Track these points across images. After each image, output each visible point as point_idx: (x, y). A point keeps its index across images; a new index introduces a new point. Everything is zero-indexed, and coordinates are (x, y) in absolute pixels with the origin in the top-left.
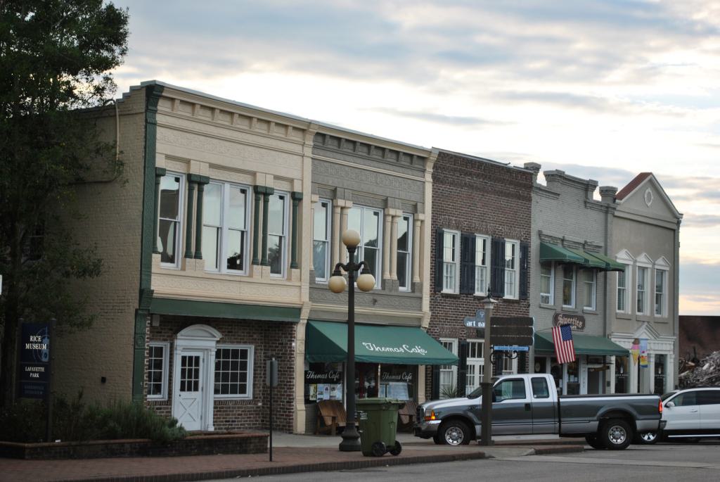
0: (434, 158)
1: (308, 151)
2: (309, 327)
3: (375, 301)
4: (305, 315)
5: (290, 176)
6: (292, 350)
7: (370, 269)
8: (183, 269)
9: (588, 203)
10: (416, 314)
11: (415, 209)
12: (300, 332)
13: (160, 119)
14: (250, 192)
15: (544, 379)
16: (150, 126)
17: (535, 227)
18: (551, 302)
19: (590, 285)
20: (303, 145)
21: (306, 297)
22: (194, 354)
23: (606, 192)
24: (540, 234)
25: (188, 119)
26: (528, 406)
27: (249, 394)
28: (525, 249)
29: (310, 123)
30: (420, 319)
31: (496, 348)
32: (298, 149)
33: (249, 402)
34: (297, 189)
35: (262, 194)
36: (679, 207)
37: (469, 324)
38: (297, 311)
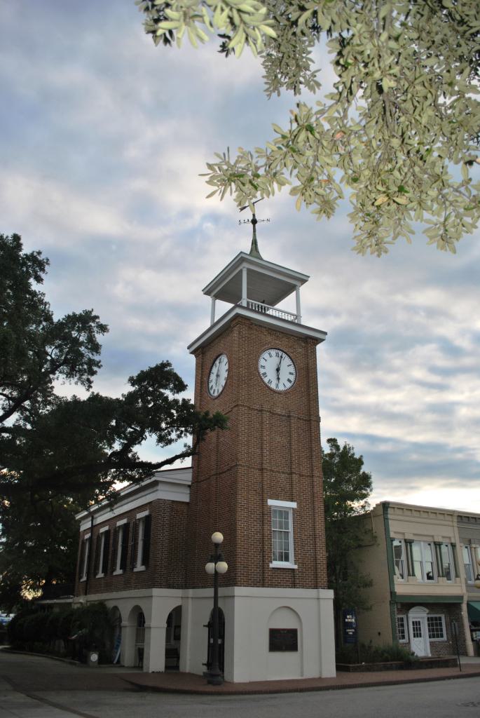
1: (455, 524)
2: (468, 605)
4: (465, 599)
6: (462, 618)
12: (464, 607)
13: (389, 516)
14: (432, 544)
16: (386, 519)
20: (452, 521)
27: (445, 638)
29: (454, 512)
32: (450, 523)
33: (446, 642)
34: (453, 541)
35: (438, 545)
38: (461, 597)
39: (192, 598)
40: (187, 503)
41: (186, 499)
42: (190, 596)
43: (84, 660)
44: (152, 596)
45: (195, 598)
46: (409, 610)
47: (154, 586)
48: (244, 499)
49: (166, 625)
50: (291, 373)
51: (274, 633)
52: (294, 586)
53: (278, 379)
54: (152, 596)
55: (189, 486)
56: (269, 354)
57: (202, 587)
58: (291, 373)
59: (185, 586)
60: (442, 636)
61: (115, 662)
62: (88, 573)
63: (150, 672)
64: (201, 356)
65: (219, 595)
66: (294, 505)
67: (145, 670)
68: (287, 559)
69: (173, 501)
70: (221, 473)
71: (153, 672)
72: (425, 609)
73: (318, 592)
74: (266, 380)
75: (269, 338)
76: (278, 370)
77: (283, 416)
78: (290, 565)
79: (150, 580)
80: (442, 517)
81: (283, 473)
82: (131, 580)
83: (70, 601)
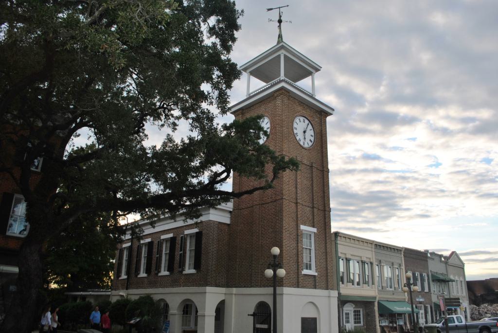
0: (403, 250)
1: (373, 250)
2: (378, 302)
3: (393, 294)
4: (377, 299)
5: (369, 257)
6: (374, 310)
7: (415, 284)
8: (347, 286)
9: (441, 261)
10: (404, 297)
11: (400, 265)
12: (376, 304)
13: (338, 242)
14: (360, 262)
15: (453, 318)
16: (336, 244)
17: (430, 269)
18: (436, 292)
19: (434, 285)
20: (372, 248)
21: (377, 294)
22: (347, 312)
23: (445, 258)
24: (431, 271)
25: (362, 246)
26: (456, 326)
27: (362, 324)
28: (428, 276)
29: (373, 241)
30: (405, 299)
31: (448, 308)
32: (370, 249)
33: (363, 326)
34: (372, 261)
35: (363, 263)
36: (464, 262)
37: (417, 300)
38: (375, 298)
39: (235, 294)
40: (228, 225)
41: (228, 221)
42: (234, 292)
44: (206, 293)
45: (238, 294)
46: (344, 305)
47: (207, 285)
48: (287, 223)
49: (215, 314)
50: (311, 136)
52: (315, 287)
53: (305, 138)
54: (206, 293)
55: (230, 212)
56: (299, 119)
57: (245, 287)
58: (311, 136)
59: (228, 285)
60: (360, 323)
64: (241, 116)
65: (449, 297)
66: (315, 230)
68: (310, 269)
69: (219, 222)
70: (263, 204)
72: (353, 305)
73: (329, 293)
75: (299, 108)
76: (305, 132)
77: (308, 166)
78: (312, 272)
79: (202, 280)
80: (366, 244)
81: (308, 207)
82: (177, 278)
83: (109, 293)
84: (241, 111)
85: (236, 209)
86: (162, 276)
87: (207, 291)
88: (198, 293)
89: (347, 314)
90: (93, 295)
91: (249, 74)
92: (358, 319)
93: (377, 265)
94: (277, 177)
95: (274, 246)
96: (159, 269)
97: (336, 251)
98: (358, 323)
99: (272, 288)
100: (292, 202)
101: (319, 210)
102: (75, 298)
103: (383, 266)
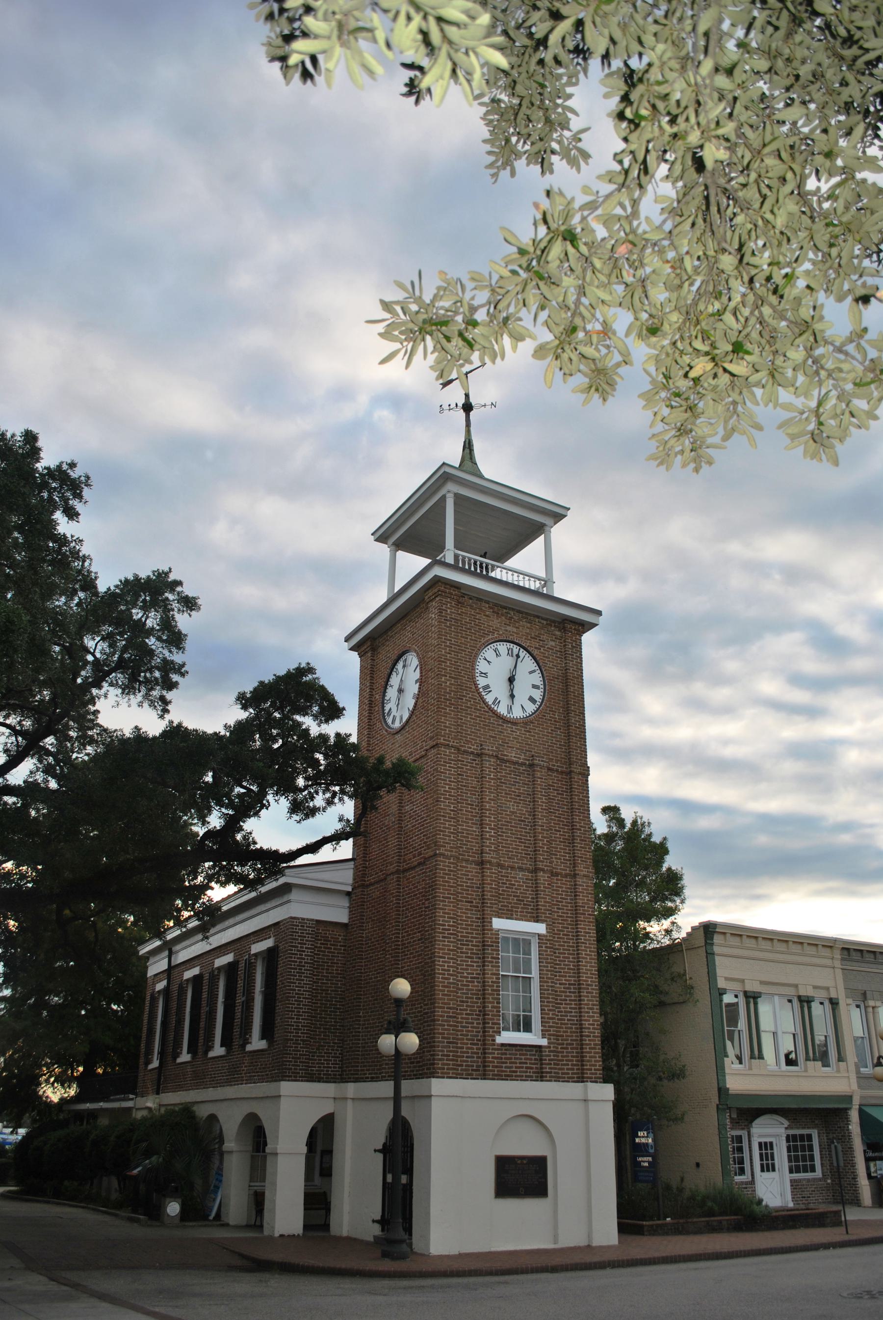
1: (838, 964)
2: (861, 1112)
4: (856, 1102)
8: (750, 1068)
12: (854, 1116)
13: (716, 949)
20: (833, 958)
22: (768, 1140)
25: (771, 951)
27: (818, 1173)
29: (835, 940)
32: (828, 962)
33: (820, 1180)
38: (849, 1098)
39: (353, 1099)
41: (343, 917)
42: (350, 1095)
43: (155, 1214)
46: (752, 1121)
47: (283, 1077)
49: (304, 1150)
50: (535, 687)
51: (503, 1164)
52: (540, 1076)
53: (512, 696)
55: (348, 894)
59: (341, 1078)
61: (211, 1218)
62: (162, 1054)
63: (277, 1235)
64: (369, 654)
66: (541, 928)
67: (266, 1232)
69: (318, 922)
71: (282, 1236)
73: (586, 1089)
74: (489, 698)
75: (495, 622)
76: (511, 680)
77: (523, 764)
81: (521, 869)
83: (130, 1104)
84: (369, 643)
85: (359, 887)
86: (255, 1051)
87: (434, 1092)
88: (244, 1098)
89: (766, 1147)
90: (106, 1110)
91: (393, 547)
92: (804, 1160)
93: (858, 1006)
94: (374, 808)
95: (398, 977)
96: (246, 1034)
97: (712, 975)
98: (805, 1171)
99: (392, 1083)
100: (467, 861)
101: (554, 874)
102: (93, 1115)
103: (873, 1008)
